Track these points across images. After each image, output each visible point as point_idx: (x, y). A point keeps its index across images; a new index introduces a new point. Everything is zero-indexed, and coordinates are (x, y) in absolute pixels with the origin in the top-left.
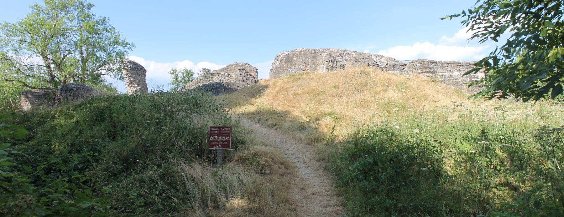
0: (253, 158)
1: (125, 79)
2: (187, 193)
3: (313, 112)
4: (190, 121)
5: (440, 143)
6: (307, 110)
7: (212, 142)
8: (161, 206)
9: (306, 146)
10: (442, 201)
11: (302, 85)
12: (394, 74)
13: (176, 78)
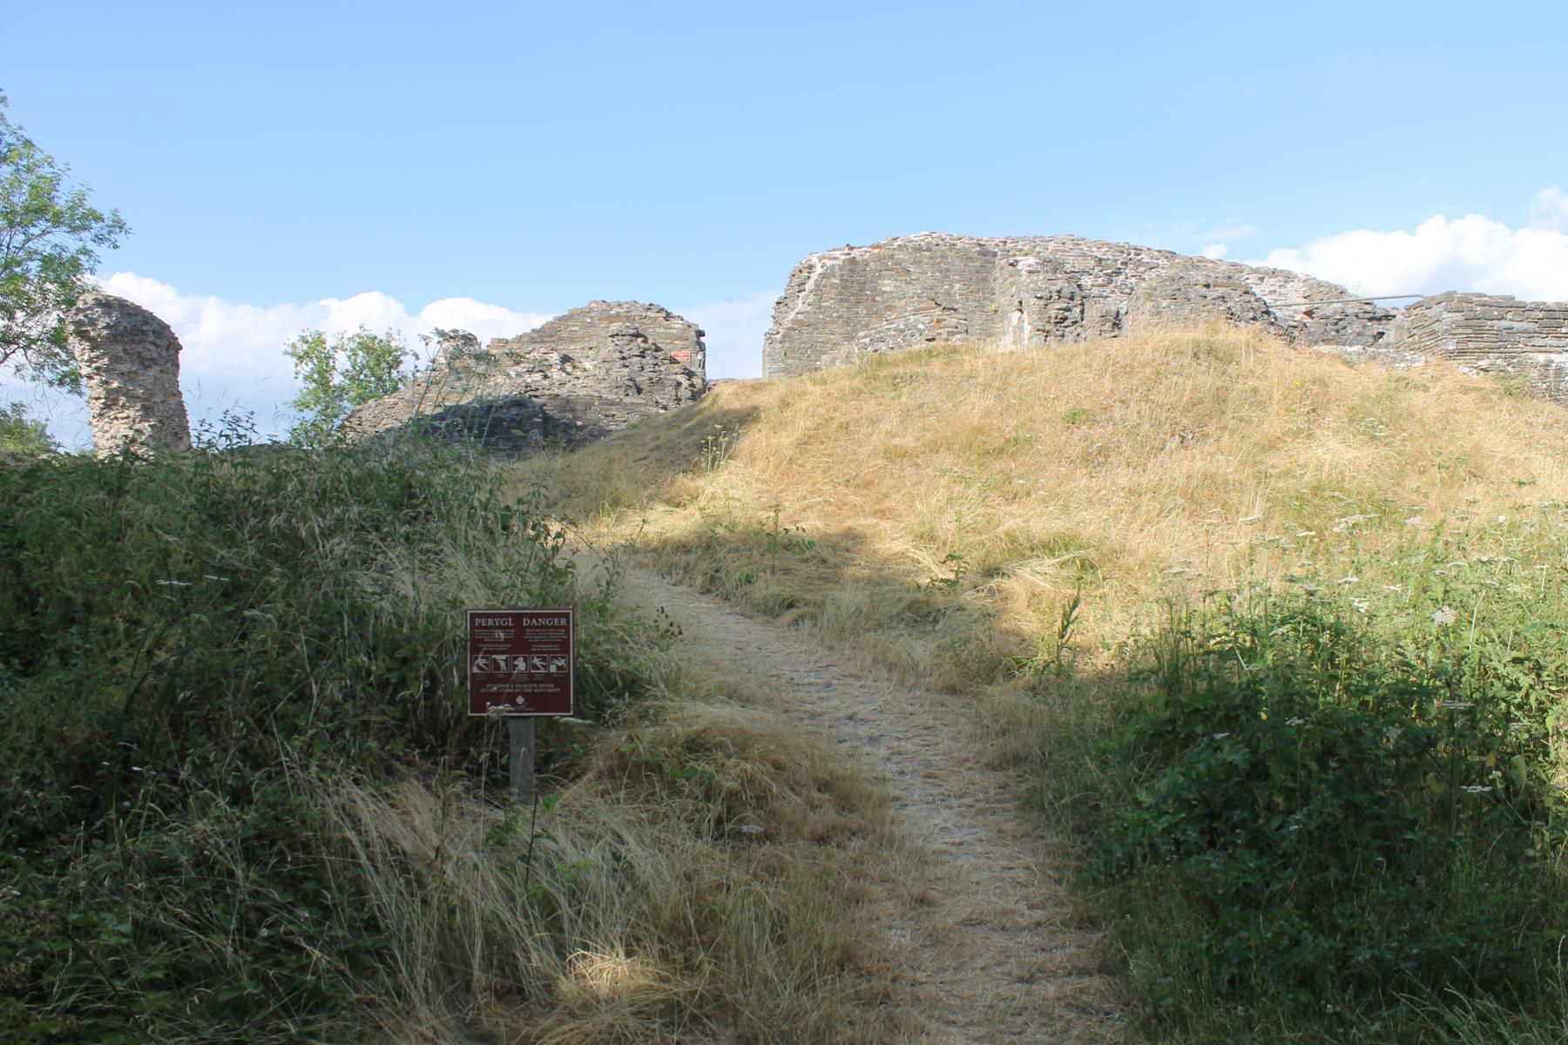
0: (682, 765)
1: (84, 381)
2: (373, 926)
3: (971, 538)
4: (375, 580)
5: (1538, 669)
6: (947, 526)
7: (483, 684)
8: (253, 984)
9: (939, 698)
10: (1541, 930)
11: (920, 407)
12: (1339, 357)
13: (322, 377)
